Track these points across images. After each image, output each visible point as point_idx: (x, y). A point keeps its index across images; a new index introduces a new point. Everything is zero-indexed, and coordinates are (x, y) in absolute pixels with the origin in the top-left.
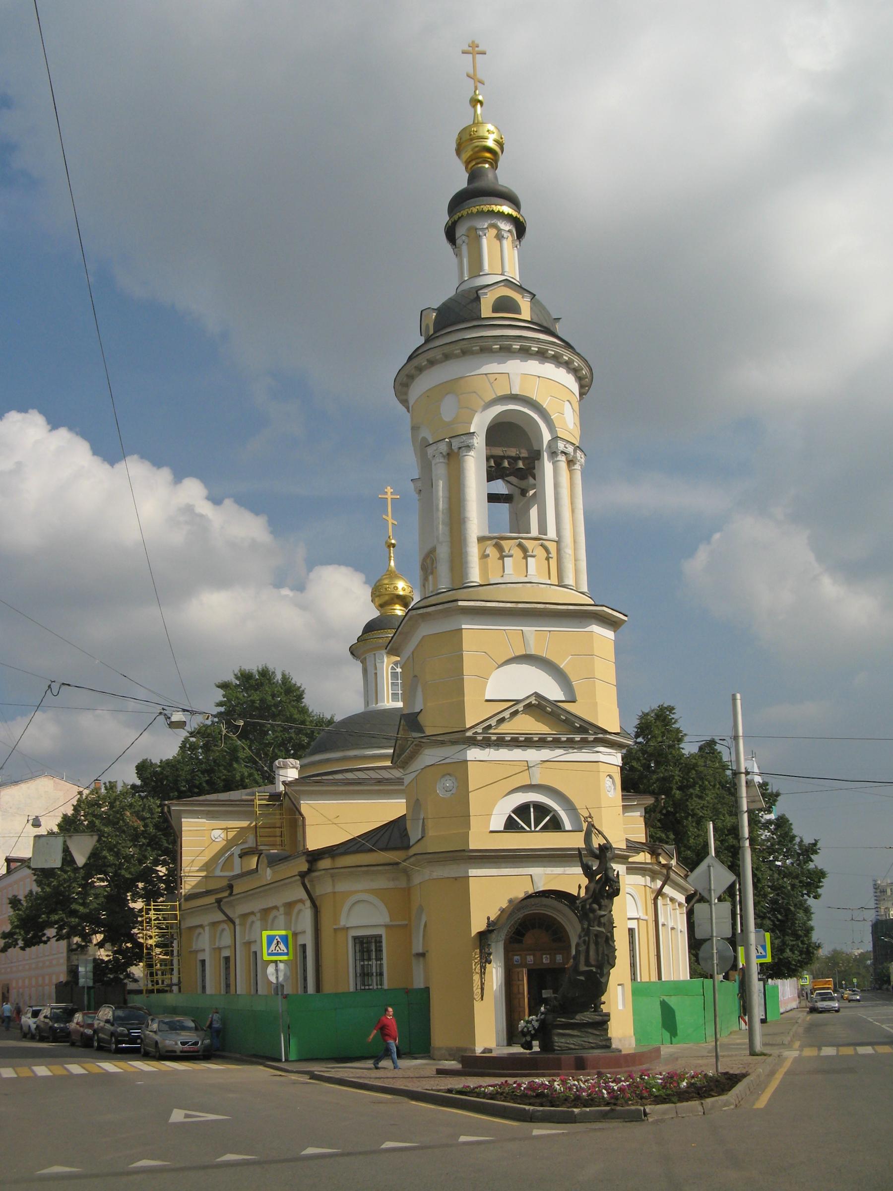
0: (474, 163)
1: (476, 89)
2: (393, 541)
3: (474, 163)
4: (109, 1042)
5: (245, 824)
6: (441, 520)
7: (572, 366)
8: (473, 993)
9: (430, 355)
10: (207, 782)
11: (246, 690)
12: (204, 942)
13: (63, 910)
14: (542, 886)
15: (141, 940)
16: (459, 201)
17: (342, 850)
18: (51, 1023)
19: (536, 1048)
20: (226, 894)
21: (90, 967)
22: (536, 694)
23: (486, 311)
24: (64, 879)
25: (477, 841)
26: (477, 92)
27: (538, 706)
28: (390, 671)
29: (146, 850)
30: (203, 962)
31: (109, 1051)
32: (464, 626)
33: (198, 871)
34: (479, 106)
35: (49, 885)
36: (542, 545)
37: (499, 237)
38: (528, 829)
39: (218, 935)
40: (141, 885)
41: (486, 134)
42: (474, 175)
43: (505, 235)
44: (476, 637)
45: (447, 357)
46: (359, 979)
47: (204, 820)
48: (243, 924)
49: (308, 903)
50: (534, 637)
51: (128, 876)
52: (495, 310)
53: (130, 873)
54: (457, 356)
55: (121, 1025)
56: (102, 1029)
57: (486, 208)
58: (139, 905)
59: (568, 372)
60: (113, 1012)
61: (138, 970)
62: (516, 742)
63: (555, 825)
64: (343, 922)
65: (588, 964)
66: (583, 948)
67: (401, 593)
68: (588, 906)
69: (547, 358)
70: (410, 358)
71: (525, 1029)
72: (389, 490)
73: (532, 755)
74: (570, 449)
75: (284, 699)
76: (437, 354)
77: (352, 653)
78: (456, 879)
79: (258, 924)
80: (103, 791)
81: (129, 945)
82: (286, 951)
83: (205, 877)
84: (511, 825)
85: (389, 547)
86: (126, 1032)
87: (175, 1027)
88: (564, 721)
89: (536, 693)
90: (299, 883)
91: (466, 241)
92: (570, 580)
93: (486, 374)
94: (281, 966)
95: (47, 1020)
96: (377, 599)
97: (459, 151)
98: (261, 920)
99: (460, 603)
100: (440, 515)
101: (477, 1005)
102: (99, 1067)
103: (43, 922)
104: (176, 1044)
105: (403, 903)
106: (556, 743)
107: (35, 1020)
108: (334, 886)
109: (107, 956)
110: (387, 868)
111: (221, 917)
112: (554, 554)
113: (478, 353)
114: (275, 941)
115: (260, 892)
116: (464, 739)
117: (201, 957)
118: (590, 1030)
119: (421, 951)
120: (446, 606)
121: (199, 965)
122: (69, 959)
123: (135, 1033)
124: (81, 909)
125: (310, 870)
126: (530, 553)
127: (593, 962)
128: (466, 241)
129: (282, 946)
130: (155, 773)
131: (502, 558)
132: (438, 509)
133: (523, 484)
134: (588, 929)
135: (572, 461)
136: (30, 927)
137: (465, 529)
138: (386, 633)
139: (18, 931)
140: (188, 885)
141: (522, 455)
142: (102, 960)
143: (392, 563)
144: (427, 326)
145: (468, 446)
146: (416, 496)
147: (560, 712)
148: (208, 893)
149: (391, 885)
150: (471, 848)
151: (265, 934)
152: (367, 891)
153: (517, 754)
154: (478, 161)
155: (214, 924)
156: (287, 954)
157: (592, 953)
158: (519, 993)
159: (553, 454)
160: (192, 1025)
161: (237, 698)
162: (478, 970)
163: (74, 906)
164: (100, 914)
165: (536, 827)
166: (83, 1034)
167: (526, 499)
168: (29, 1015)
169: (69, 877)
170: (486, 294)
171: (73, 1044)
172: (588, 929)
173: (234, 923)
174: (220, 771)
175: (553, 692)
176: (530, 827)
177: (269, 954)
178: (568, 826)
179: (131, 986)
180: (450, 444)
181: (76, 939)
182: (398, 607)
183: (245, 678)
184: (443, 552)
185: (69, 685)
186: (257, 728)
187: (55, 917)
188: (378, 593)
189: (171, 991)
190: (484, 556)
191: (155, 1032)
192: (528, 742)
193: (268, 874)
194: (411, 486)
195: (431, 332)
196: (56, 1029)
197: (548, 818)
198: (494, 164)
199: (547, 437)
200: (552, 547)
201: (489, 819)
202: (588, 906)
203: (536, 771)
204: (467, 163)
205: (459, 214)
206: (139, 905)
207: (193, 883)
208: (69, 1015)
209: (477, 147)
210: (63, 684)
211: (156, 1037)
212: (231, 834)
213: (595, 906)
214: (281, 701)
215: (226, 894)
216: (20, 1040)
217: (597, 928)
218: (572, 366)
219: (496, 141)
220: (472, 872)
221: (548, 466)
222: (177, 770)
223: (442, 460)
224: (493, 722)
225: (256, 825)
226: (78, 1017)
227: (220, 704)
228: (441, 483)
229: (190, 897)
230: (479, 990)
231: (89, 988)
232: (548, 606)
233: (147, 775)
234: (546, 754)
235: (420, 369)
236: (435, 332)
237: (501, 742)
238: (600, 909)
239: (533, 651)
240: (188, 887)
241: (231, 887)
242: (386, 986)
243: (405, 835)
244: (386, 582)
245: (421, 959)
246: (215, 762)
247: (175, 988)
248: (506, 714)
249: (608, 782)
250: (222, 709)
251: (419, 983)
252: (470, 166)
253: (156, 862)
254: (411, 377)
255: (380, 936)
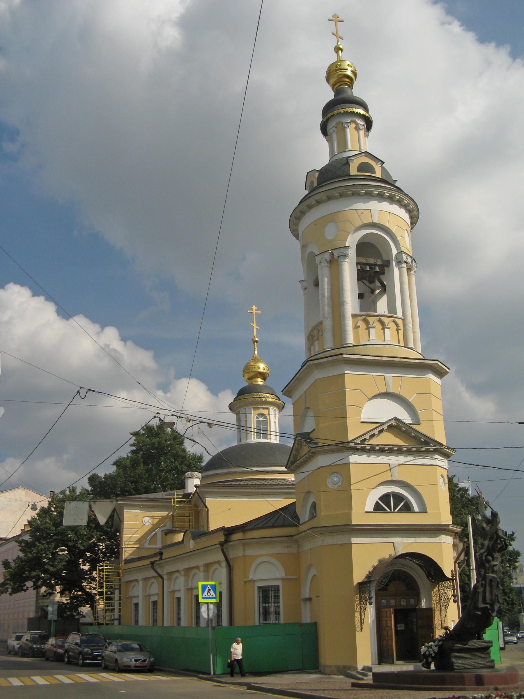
0: (338, 85)
1: (338, 41)
2: (257, 339)
3: (338, 85)
4: (78, 659)
5: (165, 514)
6: (326, 303)
7: (408, 208)
8: (355, 626)
9: (317, 197)
10: (134, 489)
11: (149, 437)
12: (138, 592)
13: (39, 569)
14: (401, 551)
15: (88, 590)
16: (329, 108)
17: (251, 527)
18: (30, 645)
19: (433, 667)
20: (158, 558)
21: (56, 607)
22: (396, 419)
23: (353, 171)
24: (41, 549)
25: (357, 519)
26: (339, 44)
27: (396, 427)
28: (255, 419)
29: (93, 531)
30: (137, 605)
31: (77, 664)
32: (346, 372)
33: (134, 544)
34: (340, 52)
35: (30, 553)
36: (394, 321)
37: (357, 128)
38: (389, 511)
39: (149, 585)
40: (88, 554)
41: (347, 67)
42: (338, 92)
43: (361, 127)
44: (353, 378)
45: (329, 198)
46: (262, 616)
47: (139, 511)
48: (169, 579)
49: (224, 564)
50: (392, 380)
51: (82, 548)
52: (359, 171)
53: (83, 546)
54: (335, 198)
55: (86, 647)
56: (73, 650)
57: (349, 110)
58: (86, 567)
59: (406, 212)
60: (80, 637)
61: (85, 609)
62: (382, 450)
63: (407, 508)
64: (251, 577)
65: (484, 601)
66: (481, 590)
67: (262, 371)
68: (484, 558)
69: (394, 201)
70: (302, 201)
71: (427, 653)
72: (254, 308)
73: (393, 460)
74: (409, 260)
75: (172, 443)
76: (323, 196)
77: (230, 409)
78: (342, 545)
79: (202, 574)
80: (68, 493)
81: (80, 593)
82: (214, 596)
83: (138, 548)
84: (378, 508)
85: (254, 342)
86: (90, 651)
87: (127, 649)
88: (413, 437)
89: (395, 417)
90: (220, 549)
91: (336, 131)
92: (411, 345)
93: (355, 210)
94: (211, 606)
95: (27, 642)
96: (246, 375)
97: (328, 79)
98: (185, 575)
99: (345, 356)
100: (326, 300)
101: (358, 635)
102: (55, 678)
103: (26, 576)
104: (131, 661)
105: (294, 564)
106: (409, 452)
107: (18, 642)
108: (244, 551)
109: (66, 600)
110: (283, 539)
111: (153, 574)
112: (401, 327)
113: (350, 196)
114: (207, 589)
115: (185, 557)
116: (346, 447)
117: (135, 601)
118: (478, 654)
119: (307, 596)
120: (335, 358)
121: (133, 607)
122: (37, 601)
123: (96, 652)
124: (51, 569)
125: (226, 541)
126: (386, 326)
127: (488, 600)
128: (336, 131)
129: (212, 592)
130: (101, 482)
131: (368, 328)
132: (324, 297)
133: (372, 286)
134: (485, 575)
135: (410, 268)
136: (17, 579)
137: (344, 309)
138: (253, 395)
139: (9, 582)
140: (127, 553)
141: (378, 263)
142: (63, 603)
143: (256, 353)
144: (312, 183)
145: (345, 255)
146: (302, 292)
147: (411, 430)
148: (140, 559)
149: (286, 551)
150: (353, 523)
151: (200, 584)
152: (269, 555)
153: (383, 459)
154: (341, 83)
155: (146, 579)
156: (215, 598)
157: (488, 594)
158: (387, 626)
159: (399, 263)
160: (137, 646)
161: (144, 442)
162: (358, 610)
163: (46, 567)
164: (62, 573)
165: (394, 509)
166: (56, 653)
167: (373, 296)
168: (14, 639)
169: (45, 547)
170: (353, 160)
171: (47, 659)
172: (485, 575)
173: (162, 578)
174: (142, 482)
175: (406, 418)
176: (390, 509)
177: (203, 598)
178: (416, 509)
179: (82, 620)
180: (332, 254)
181: (44, 589)
182: (260, 380)
183: (149, 429)
184: (328, 324)
185: (93, 391)
186: (156, 461)
187: (34, 574)
188: (247, 371)
189: (113, 624)
190: (356, 327)
191: (115, 652)
192: (390, 450)
193: (192, 544)
194: (299, 285)
195: (315, 185)
196: (35, 648)
197: (402, 503)
198: (351, 86)
199: (394, 252)
200: (400, 322)
201: (364, 505)
202: (484, 558)
203: (395, 470)
204: (333, 86)
205: (332, 114)
206: (86, 567)
207: (130, 552)
208: (44, 639)
209: (341, 75)
210: (89, 390)
211: (116, 656)
212: (156, 521)
213: (490, 558)
214: (171, 444)
215: (158, 558)
216: (5, 655)
217: (491, 575)
218: (408, 208)
219: (352, 71)
220: (354, 540)
221: (396, 270)
222: (116, 480)
223: (326, 264)
224: (367, 437)
225: (172, 514)
226: (52, 641)
227: (132, 445)
228: (326, 279)
229: (127, 561)
230: (359, 624)
231: (54, 621)
232: (402, 359)
233: (96, 483)
234: (402, 459)
235: (310, 207)
236: (318, 185)
237: (373, 450)
238: (493, 560)
239: (391, 390)
240: (127, 554)
241: (161, 554)
242: (282, 621)
243: (296, 517)
244: (252, 364)
245: (308, 603)
246: (139, 476)
247: (116, 622)
248: (376, 432)
249: (441, 480)
250: (134, 448)
251: (307, 619)
252: (336, 87)
253: (99, 540)
254: (303, 213)
255: (278, 587)
